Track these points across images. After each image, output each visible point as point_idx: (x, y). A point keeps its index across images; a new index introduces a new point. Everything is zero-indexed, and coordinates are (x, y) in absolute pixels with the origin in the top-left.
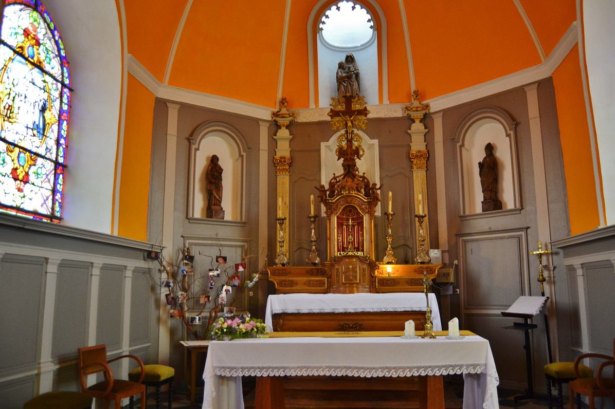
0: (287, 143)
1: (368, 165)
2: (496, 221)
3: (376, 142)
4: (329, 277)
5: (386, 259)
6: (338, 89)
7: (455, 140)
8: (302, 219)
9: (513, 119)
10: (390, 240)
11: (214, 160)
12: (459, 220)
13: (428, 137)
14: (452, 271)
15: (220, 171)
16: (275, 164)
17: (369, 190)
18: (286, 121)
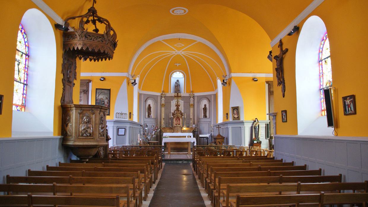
0: (164, 101)
1: (182, 108)
2: (205, 120)
3: (183, 101)
4: (174, 130)
5: (184, 127)
6: (175, 88)
7: (199, 102)
8: (167, 118)
9: (209, 101)
10: (185, 123)
11: (149, 105)
12: (199, 119)
13: (194, 101)
14: (197, 129)
15: (151, 108)
16: (162, 105)
17: (181, 114)
18: (164, 96)
